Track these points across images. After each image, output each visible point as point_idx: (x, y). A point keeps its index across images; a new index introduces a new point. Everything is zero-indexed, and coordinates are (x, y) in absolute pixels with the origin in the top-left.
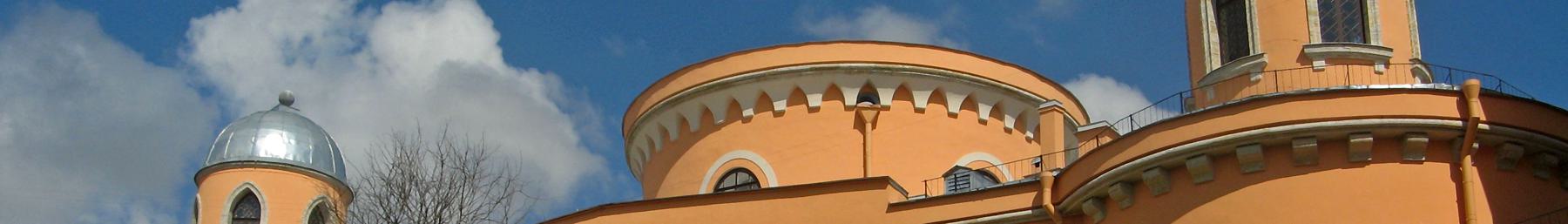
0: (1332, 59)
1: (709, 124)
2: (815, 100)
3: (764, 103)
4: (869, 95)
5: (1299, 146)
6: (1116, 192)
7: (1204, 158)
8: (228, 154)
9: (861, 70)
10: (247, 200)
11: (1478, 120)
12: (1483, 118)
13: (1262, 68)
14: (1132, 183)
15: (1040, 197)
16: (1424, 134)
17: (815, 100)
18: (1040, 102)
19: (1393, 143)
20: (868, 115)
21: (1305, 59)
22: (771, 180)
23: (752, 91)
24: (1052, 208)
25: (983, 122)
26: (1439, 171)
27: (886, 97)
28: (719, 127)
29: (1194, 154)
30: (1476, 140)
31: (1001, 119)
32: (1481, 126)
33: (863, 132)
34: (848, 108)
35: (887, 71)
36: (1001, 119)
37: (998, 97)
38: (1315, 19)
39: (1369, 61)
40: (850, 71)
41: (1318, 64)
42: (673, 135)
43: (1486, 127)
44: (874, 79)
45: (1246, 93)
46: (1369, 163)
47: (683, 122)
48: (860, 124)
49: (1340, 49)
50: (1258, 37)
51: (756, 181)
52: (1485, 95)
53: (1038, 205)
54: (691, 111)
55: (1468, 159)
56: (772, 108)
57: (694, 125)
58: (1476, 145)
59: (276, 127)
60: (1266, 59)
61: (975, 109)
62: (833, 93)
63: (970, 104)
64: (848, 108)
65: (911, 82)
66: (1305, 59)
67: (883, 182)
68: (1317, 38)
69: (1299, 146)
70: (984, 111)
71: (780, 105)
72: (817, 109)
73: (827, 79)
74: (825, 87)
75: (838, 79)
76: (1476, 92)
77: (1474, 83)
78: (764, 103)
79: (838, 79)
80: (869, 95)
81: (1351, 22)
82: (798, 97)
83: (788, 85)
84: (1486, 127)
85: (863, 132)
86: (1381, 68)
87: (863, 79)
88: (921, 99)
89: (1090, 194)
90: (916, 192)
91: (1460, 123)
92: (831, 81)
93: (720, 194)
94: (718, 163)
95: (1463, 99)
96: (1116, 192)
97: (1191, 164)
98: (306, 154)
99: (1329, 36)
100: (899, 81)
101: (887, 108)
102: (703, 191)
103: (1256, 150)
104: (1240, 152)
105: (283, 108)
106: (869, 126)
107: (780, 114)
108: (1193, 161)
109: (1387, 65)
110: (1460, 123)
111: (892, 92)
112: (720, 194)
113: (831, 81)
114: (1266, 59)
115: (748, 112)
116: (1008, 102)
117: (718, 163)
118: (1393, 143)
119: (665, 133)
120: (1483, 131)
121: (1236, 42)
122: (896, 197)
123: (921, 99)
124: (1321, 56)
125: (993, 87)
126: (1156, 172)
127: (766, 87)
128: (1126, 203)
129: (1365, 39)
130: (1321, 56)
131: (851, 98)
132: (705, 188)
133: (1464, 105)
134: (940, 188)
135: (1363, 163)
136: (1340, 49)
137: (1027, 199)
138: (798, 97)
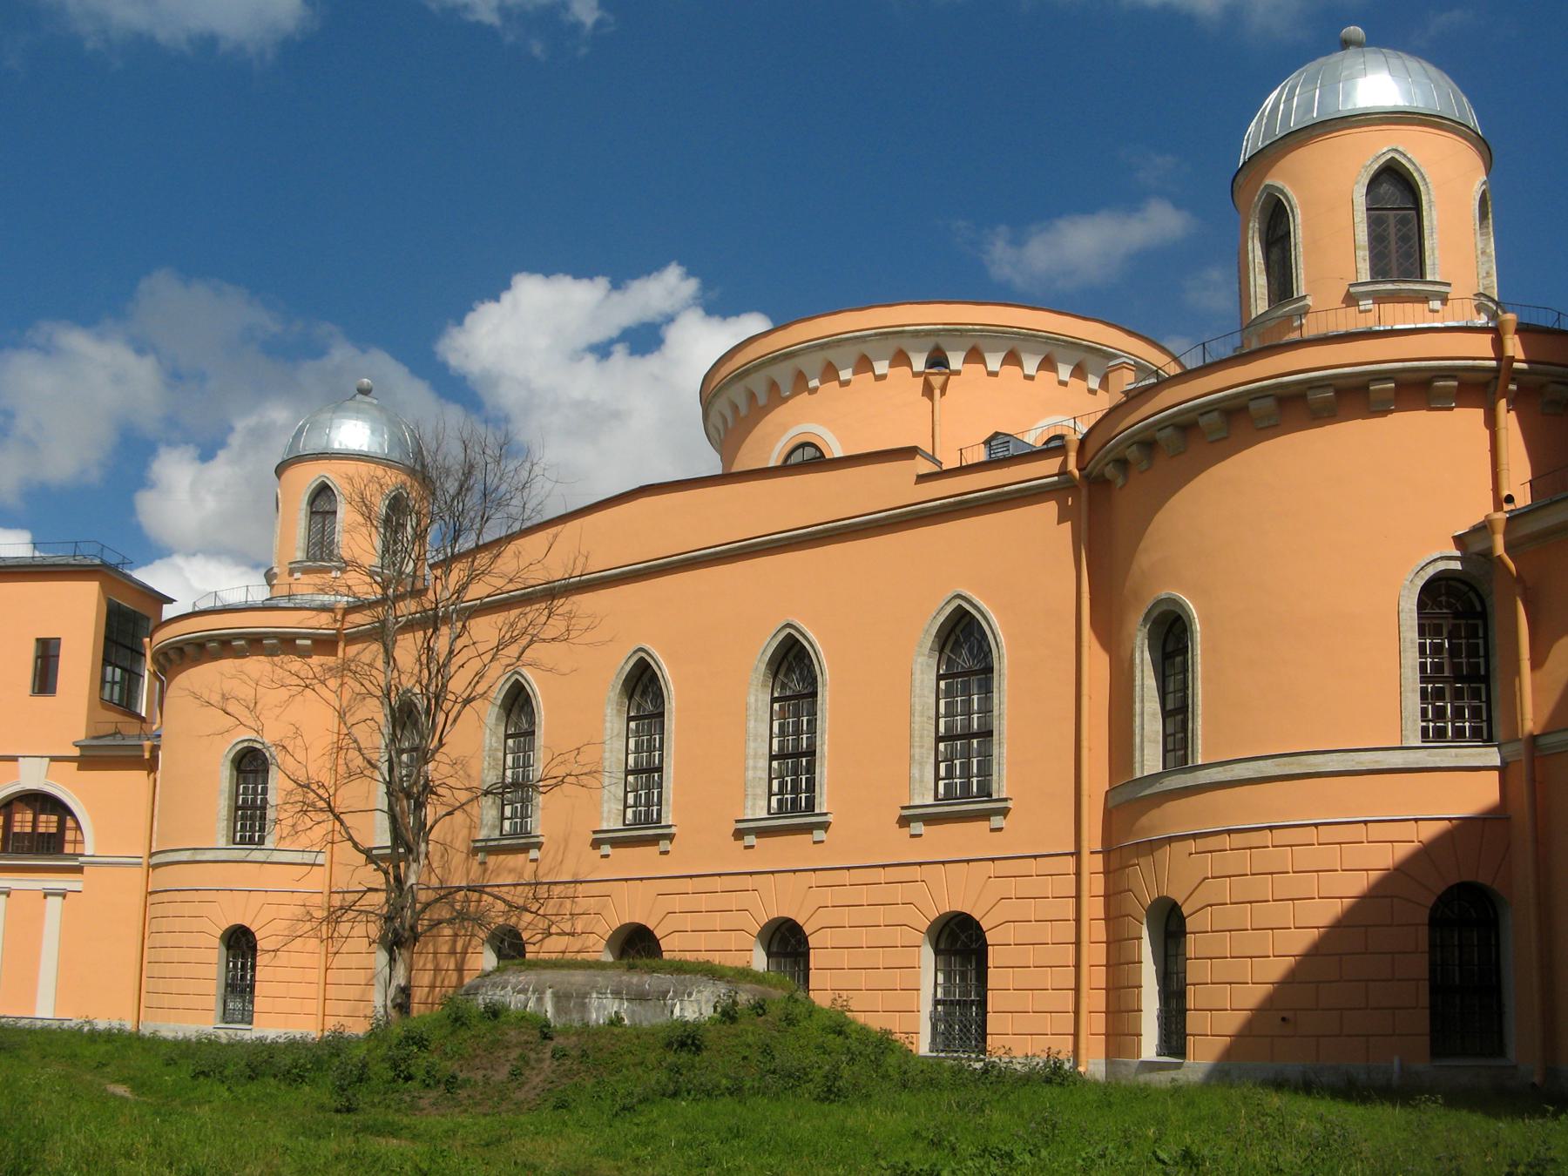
0: (1380, 298)
1: (776, 397)
2: (881, 367)
3: (830, 372)
4: (938, 360)
5: (1314, 396)
6: (1132, 453)
7: (1216, 414)
8: (309, 445)
9: (928, 333)
10: (323, 491)
11: (1512, 359)
12: (1520, 355)
13: (1305, 311)
14: (1148, 444)
15: (1065, 463)
16: (1453, 378)
17: (881, 367)
18: (1116, 356)
19: (1419, 388)
20: (937, 381)
21: (1351, 300)
22: (836, 450)
23: (818, 359)
24: (1076, 473)
25: (1063, 383)
26: (1470, 419)
27: (956, 361)
28: (785, 400)
29: (1205, 410)
30: (1513, 380)
31: (1085, 379)
32: (1516, 365)
33: (931, 398)
34: (916, 375)
35: (956, 333)
36: (1085, 379)
37: (1079, 356)
38: (1364, 254)
39: (1424, 298)
40: (916, 334)
41: (1366, 304)
42: (743, 411)
43: (1525, 366)
44: (943, 342)
45: (1295, 336)
46: (1392, 412)
47: (752, 396)
48: (928, 391)
49: (1390, 286)
50: (1302, 276)
51: (823, 455)
52: (1523, 330)
53: (1063, 472)
54: (758, 383)
55: (1503, 403)
56: (911, 367)
57: (762, 400)
58: (1513, 387)
59: (350, 418)
60: (1309, 301)
61: (1054, 369)
62: (901, 359)
63: (1048, 364)
64: (916, 375)
65: (981, 343)
66: (1351, 300)
67: (910, 452)
68: (1365, 276)
69: (1314, 396)
70: (1064, 372)
71: (845, 374)
72: (883, 377)
73: (893, 344)
74: (969, 346)
75: (904, 343)
76: (1511, 327)
77: (1510, 318)
78: (830, 372)
79: (904, 343)
80: (938, 360)
81: (1409, 256)
82: (864, 364)
83: (852, 352)
84: (1525, 366)
85: (931, 398)
86: (1436, 304)
87: (930, 343)
88: (994, 362)
89: (1109, 458)
90: (950, 462)
91: (1494, 363)
92: (898, 347)
93: (786, 468)
94: (785, 439)
95: (1497, 333)
96: (1132, 453)
97: (1203, 421)
98: (381, 446)
99: (1380, 269)
100: (969, 343)
101: (958, 373)
102: (771, 464)
103: (1269, 403)
104: (1253, 406)
105: (359, 397)
106: (937, 393)
107: (846, 383)
108: (1206, 417)
109: (1444, 299)
110: (1494, 363)
111: (961, 355)
112: (786, 468)
113: (898, 347)
114: (1309, 301)
115: (814, 383)
116: (1091, 361)
117: (785, 439)
118: (1419, 388)
119: (735, 408)
120: (1521, 371)
121: (1282, 287)
122: (925, 467)
123: (994, 362)
124: (1367, 295)
125: (1073, 345)
126: (1168, 431)
127: (831, 355)
128: (1144, 465)
129: (1422, 274)
130: (1367, 295)
131: (919, 363)
132: (774, 460)
133: (1498, 344)
134: (981, 455)
135: (1384, 413)
136: (1390, 286)
137: (1051, 466)
138: (864, 364)
